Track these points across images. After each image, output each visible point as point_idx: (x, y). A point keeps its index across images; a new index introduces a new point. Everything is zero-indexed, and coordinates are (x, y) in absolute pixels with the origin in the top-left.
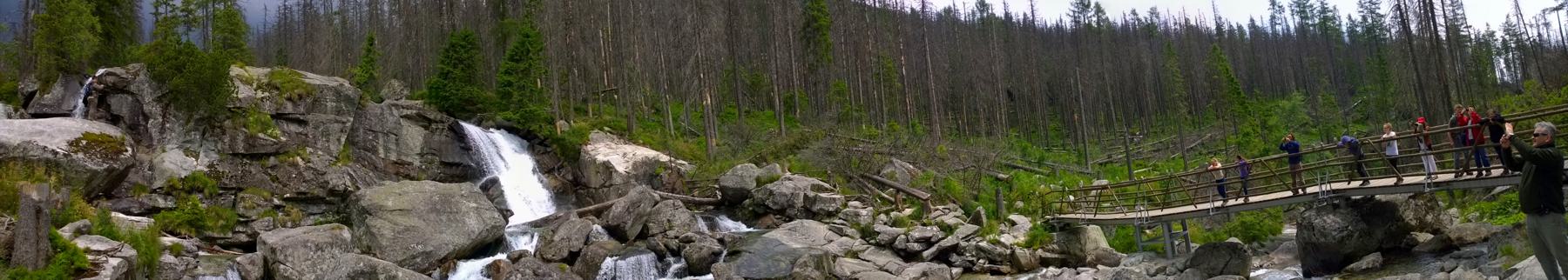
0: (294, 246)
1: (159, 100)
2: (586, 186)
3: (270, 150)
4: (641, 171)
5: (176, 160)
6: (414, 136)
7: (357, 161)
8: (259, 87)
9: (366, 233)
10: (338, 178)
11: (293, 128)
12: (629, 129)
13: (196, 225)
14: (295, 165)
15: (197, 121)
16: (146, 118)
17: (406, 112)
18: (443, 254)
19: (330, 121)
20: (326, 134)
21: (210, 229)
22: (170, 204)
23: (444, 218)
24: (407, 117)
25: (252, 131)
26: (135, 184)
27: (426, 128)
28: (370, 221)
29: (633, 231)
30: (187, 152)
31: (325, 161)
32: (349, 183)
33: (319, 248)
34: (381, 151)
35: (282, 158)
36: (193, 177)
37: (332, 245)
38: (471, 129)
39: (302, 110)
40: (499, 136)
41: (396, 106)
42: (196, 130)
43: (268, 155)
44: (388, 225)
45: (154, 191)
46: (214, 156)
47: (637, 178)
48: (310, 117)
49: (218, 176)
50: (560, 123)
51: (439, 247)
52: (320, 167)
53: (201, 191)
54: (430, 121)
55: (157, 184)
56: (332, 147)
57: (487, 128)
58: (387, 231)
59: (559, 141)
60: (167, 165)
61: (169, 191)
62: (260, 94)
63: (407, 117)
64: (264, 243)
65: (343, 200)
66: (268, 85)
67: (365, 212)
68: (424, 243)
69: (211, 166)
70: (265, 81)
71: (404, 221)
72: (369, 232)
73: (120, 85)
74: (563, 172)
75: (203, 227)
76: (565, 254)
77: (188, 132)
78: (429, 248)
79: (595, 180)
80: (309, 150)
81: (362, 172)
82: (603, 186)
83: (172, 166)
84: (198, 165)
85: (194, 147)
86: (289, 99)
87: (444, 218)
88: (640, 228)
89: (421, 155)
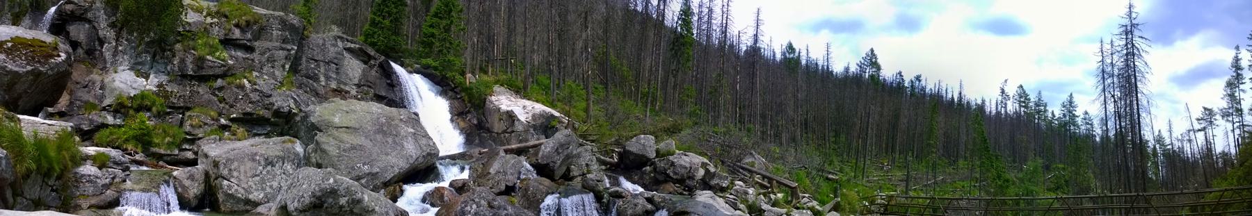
0: (241, 159)
1: (112, 25)
2: (489, 131)
3: (218, 71)
4: (539, 122)
5: (125, 81)
6: (354, 68)
7: (300, 87)
8: (209, 14)
9: (315, 151)
10: (284, 100)
11: (240, 54)
12: (525, 88)
13: (143, 140)
14: (242, 87)
15: (148, 44)
16: (102, 43)
17: (349, 45)
18: (389, 176)
19: (276, 49)
20: (271, 60)
21: (158, 145)
22: (118, 121)
23: (390, 140)
24: (349, 50)
25: (201, 52)
26: (87, 102)
27: (365, 63)
28: (320, 137)
29: (559, 173)
30: (139, 74)
31: (268, 83)
32: (293, 106)
33: (269, 162)
34: (322, 79)
35: (228, 79)
36: (143, 96)
37: (283, 159)
38: (397, 68)
39: (249, 36)
40: (417, 78)
41: (341, 38)
42: (147, 52)
43: (216, 77)
44: (333, 142)
45: (104, 109)
46: (164, 78)
47: (535, 127)
48: (257, 44)
49: (166, 95)
50: (469, 75)
51: (385, 170)
52: (266, 89)
53: (149, 109)
54: (370, 57)
55: (107, 102)
56: (277, 73)
57: (411, 72)
58: (332, 150)
59: (467, 90)
60: (117, 84)
61: (120, 108)
62: (209, 20)
63: (349, 50)
64: (206, 156)
65: (287, 122)
66: (217, 13)
67: (315, 128)
68: (370, 163)
69: (160, 86)
70: (214, 9)
71: (350, 139)
72: (319, 148)
73: (78, 13)
74: (469, 116)
75: (150, 144)
76: (503, 188)
77: (139, 55)
78: (376, 170)
79: (498, 127)
80: (255, 74)
81: (305, 97)
82: (505, 132)
83: (122, 86)
84: (150, 84)
85: (146, 68)
86: (237, 26)
87: (390, 140)
88: (564, 168)
89: (358, 86)
